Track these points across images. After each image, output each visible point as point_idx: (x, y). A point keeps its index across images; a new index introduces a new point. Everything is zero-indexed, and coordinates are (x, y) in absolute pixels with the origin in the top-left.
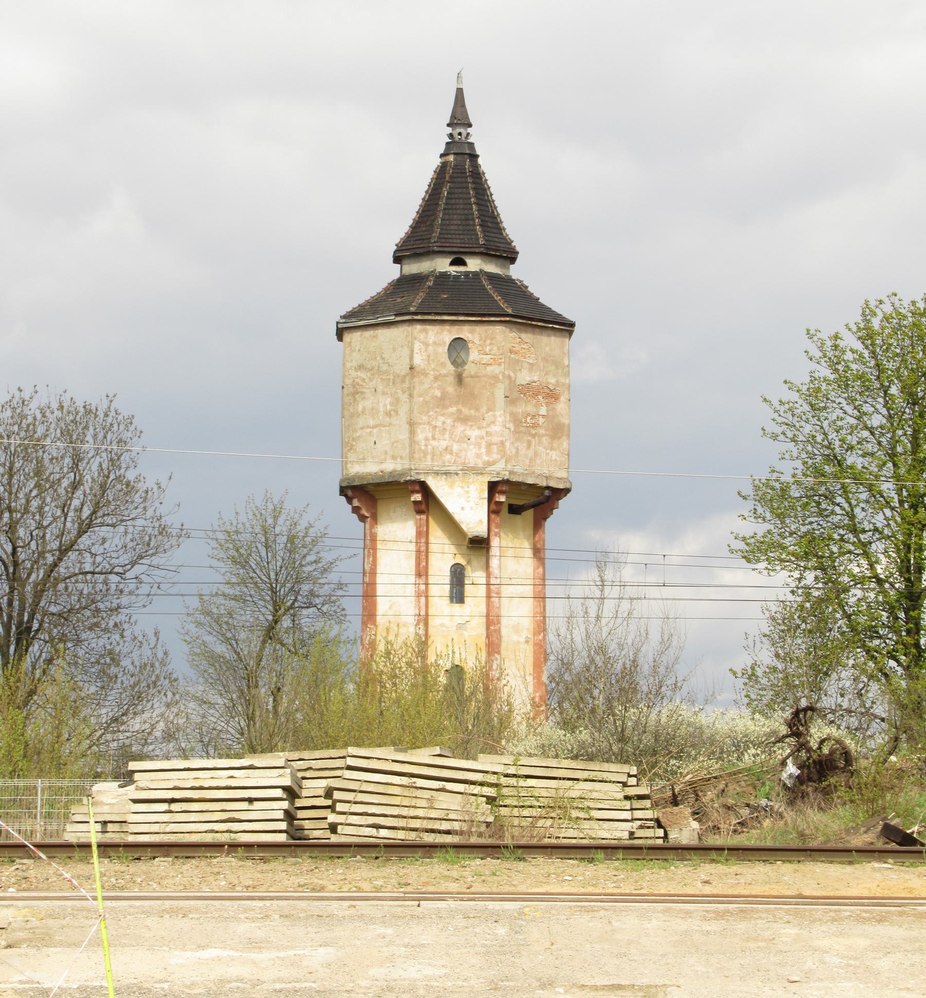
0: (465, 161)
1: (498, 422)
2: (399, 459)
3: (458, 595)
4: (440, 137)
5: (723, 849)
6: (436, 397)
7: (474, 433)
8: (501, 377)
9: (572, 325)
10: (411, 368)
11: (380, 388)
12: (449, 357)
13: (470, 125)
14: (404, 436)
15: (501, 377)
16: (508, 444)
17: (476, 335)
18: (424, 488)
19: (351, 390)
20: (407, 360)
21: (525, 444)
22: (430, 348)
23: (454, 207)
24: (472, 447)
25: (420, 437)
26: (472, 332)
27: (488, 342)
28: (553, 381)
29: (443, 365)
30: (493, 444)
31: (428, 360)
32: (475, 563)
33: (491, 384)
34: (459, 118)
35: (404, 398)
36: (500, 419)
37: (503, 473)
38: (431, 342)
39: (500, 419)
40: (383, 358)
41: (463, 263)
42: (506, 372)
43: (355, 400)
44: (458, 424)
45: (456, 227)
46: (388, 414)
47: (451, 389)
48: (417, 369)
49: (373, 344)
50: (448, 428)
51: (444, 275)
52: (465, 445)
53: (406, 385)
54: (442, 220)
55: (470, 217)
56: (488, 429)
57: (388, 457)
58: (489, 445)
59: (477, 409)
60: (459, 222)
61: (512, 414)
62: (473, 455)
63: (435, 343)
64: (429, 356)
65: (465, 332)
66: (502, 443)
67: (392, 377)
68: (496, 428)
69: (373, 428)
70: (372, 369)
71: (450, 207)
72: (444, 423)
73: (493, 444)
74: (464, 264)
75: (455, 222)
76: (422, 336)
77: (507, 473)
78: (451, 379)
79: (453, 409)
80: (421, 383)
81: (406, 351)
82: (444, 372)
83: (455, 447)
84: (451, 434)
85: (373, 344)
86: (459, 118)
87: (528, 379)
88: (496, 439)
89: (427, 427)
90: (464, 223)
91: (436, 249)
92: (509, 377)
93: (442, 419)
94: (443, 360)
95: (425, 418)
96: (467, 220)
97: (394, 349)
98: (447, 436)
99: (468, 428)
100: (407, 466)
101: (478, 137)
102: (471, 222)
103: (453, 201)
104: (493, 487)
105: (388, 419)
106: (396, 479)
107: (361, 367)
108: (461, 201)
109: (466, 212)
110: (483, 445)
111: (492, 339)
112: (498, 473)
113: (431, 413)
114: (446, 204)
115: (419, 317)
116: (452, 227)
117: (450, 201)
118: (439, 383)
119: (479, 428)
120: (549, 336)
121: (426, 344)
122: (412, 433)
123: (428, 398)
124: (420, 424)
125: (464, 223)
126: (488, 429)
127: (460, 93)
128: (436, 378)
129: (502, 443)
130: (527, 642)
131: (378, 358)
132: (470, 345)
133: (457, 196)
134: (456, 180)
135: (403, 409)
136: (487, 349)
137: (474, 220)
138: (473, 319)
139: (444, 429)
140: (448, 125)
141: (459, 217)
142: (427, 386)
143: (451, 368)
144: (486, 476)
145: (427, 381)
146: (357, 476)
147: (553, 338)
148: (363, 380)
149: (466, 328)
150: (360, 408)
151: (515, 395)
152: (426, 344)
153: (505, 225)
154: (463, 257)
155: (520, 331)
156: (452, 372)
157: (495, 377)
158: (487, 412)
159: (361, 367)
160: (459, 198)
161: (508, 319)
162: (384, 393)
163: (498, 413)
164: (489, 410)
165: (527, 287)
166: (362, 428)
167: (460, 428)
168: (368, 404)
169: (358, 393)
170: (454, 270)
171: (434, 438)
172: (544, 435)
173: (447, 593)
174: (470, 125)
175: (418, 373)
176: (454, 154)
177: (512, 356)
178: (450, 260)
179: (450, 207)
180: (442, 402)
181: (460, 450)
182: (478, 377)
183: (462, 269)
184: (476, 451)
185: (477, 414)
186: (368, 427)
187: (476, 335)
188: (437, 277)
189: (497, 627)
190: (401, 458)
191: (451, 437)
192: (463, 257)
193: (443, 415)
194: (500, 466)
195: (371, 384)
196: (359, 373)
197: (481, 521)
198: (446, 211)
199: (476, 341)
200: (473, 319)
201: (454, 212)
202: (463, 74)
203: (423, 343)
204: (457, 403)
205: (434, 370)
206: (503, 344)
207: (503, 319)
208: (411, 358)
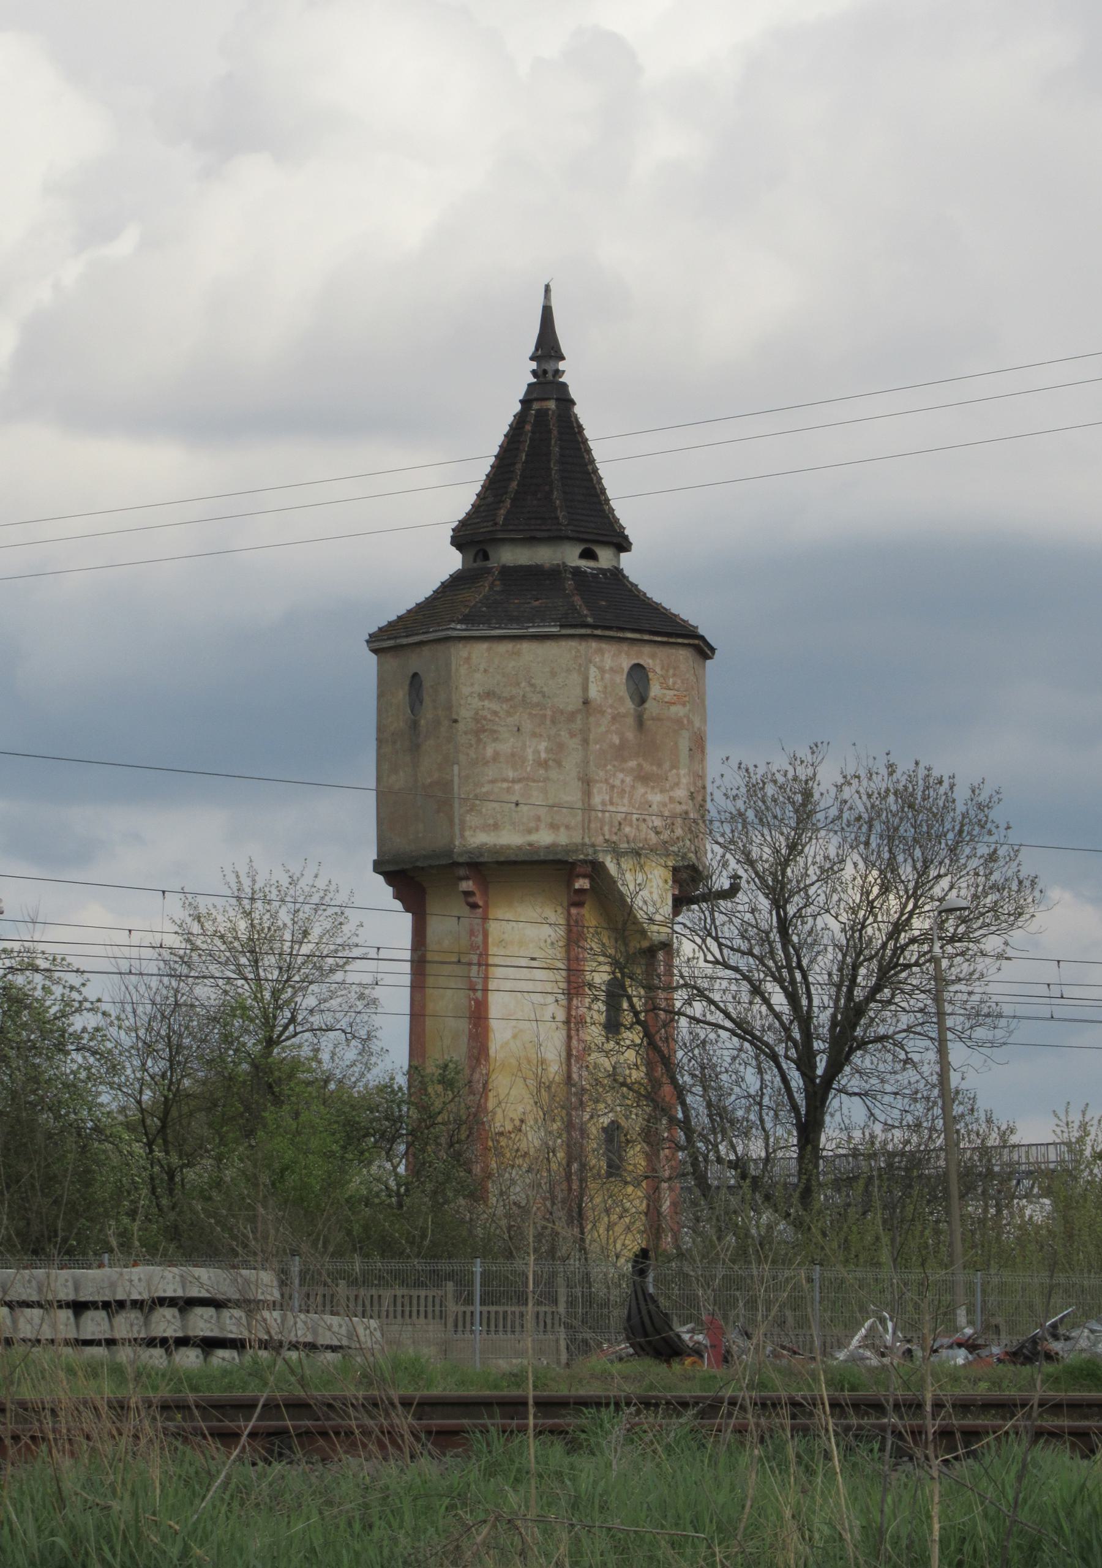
2: (562, 829)
5: (685, 1405)
8: (685, 722)
9: (713, 650)
10: (586, 702)
11: (528, 726)
13: (563, 358)
14: (572, 795)
15: (685, 722)
18: (596, 870)
20: (578, 691)
22: (607, 676)
25: (597, 800)
26: (653, 656)
27: (671, 672)
29: (621, 700)
31: (605, 693)
34: (547, 348)
35: (573, 743)
36: (684, 781)
40: (532, 685)
43: (479, 741)
44: (639, 785)
46: (544, 764)
47: (630, 735)
49: (512, 664)
50: (628, 789)
51: (577, 572)
53: (578, 724)
56: (671, 794)
57: (543, 825)
59: (660, 765)
63: (611, 669)
64: (605, 687)
67: (549, 713)
69: (513, 781)
70: (512, 698)
72: (623, 781)
78: (630, 721)
79: (632, 764)
81: (576, 678)
82: (622, 710)
84: (631, 798)
86: (547, 348)
89: (604, 787)
91: (570, 533)
93: (621, 776)
94: (621, 694)
95: (602, 773)
97: (553, 674)
98: (626, 801)
100: (578, 840)
101: (574, 373)
105: (542, 771)
106: (559, 857)
107: (489, 695)
111: (675, 669)
113: (609, 767)
115: (598, 632)
119: (662, 791)
122: (588, 794)
124: (597, 781)
126: (671, 794)
128: (614, 718)
131: (523, 684)
132: (651, 675)
135: (572, 762)
138: (659, 639)
139: (623, 791)
140: (532, 359)
142: (603, 729)
145: (605, 720)
146: (480, 850)
148: (495, 713)
149: (647, 649)
150: (489, 752)
152: (602, 670)
157: (679, 721)
158: (670, 770)
159: (489, 695)
162: (534, 735)
166: (493, 782)
168: (505, 747)
169: (485, 731)
170: (584, 564)
171: (612, 803)
174: (563, 358)
176: (557, 400)
180: (620, 752)
183: (592, 564)
186: (504, 780)
190: (567, 827)
193: (622, 770)
195: (510, 720)
196: (486, 703)
199: (658, 670)
200: (659, 639)
203: (598, 668)
205: (611, 706)
208: (585, 689)
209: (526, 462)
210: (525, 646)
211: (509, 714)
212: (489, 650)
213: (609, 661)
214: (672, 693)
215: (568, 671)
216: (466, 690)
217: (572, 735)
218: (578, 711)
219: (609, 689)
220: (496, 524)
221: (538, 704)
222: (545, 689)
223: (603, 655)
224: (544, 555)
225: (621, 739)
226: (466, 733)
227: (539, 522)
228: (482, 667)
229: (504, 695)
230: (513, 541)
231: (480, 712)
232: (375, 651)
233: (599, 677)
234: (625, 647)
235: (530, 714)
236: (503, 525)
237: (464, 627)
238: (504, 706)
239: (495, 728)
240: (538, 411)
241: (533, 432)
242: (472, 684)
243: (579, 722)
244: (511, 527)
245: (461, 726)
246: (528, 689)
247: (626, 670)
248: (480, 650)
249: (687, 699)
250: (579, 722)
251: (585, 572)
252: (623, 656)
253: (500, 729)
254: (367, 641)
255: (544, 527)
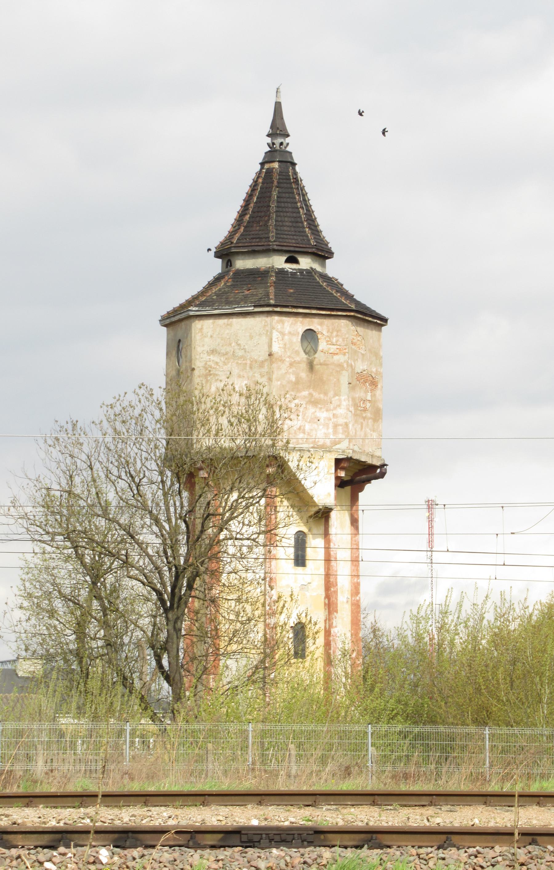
0: (288, 168)
1: (343, 406)
3: (300, 560)
4: (261, 146)
6: (292, 381)
7: (323, 415)
8: (345, 366)
9: (385, 320)
10: (270, 355)
11: (236, 371)
12: (302, 346)
13: (288, 136)
15: (345, 366)
16: (350, 426)
17: (325, 327)
19: (203, 372)
20: (266, 347)
21: (360, 426)
22: (286, 337)
23: (284, 210)
24: (321, 427)
26: (321, 324)
27: (335, 334)
28: (374, 370)
29: (297, 353)
30: (339, 425)
31: (285, 348)
32: (315, 531)
33: (337, 371)
34: (278, 129)
36: (344, 403)
37: (348, 451)
38: (286, 332)
39: (344, 403)
40: (239, 345)
41: (296, 261)
42: (350, 362)
43: (207, 381)
45: (288, 229)
47: (304, 375)
48: (275, 356)
49: (227, 331)
51: (281, 272)
52: (315, 426)
53: (265, 369)
54: (276, 221)
55: (299, 220)
56: (334, 412)
58: (336, 426)
59: (326, 394)
60: (290, 224)
61: (354, 399)
62: (322, 433)
64: (285, 345)
65: (315, 324)
66: (346, 425)
67: (248, 362)
68: (341, 411)
70: (227, 353)
71: (280, 209)
73: (339, 425)
74: (296, 261)
75: (287, 224)
76: (279, 326)
77: (351, 451)
79: (305, 393)
80: (279, 368)
81: (264, 339)
82: (298, 359)
83: (307, 427)
84: (304, 415)
85: (227, 331)
86: (278, 129)
87: (361, 368)
88: (341, 421)
90: (294, 224)
92: (351, 366)
94: (297, 348)
96: (297, 222)
97: (251, 337)
99: (318, 410)
101: (295, 146)
102: (300, 225)
103: (283, 205)
104: (338, 462)
107: (213, 352)
108: (289, 205)
109: (295, 215)
110: (331, 425)
111: (337, 332)
112: (343, 452)
114: (277, 207)
115: (278, 309)
116: (285, 228)
117: (280, 205)
118: (294, 369)
119: (327, 410)
120: (372, 330)
121: (283, 334)
123: (284, 382)
125: (294, 224)
126: (334, 412)
127: (278, 107)
128: (291, 365)
129: (346, 425)
130: (347, 602)
131: (233, 344)
133: (285, 200)
134: (282, 185)
136: (334, 340)
137: (302, 223)
138: (324, 312)
140: (268, 135)
141: (290, 220)
142: (283, 371)
143: (303, 356)
144: (333, 453)
145: (284, 367)
147: (374, 332)
148: (217, 363)
149: (316, 321)
151: (355, 382)
152: (283, 334)
153: (321, 228)
154: (296, 256)
155: (357, 325)
156: (305, 360)
157: (340, 365)
158: (334, 396)
159: (213, 352)
160: (287, 202)
161: (352, 314)
162: (239, 376)
163: (343, 398)
164: (336, 395)
165: (342, 285)
167: (311, 410)
169: (210, 375)
170: (289, 267)
172: (370, 418)
173: (292, 557)
174: (288, 136)
175: (276, 359)
176: (279, 161)
177: (353, 347)
178: (285, 258)
179: (280, 209)
181: (311, 430)
182: (327, 365)
183: (294, 266)
184: (324, 430)
185: (326, 398)
187: (325, 327)
188: (277, 273)
189: (335, 589)
191: (303, 418)
192: (296, 256)
194: (344, 445)
195: (225, 367)
197: (329, 494)
198: (278, 214)
199: (325, 332)
200: (324, 312)
201: (285, 214)
202: (281, 89)
204: (309, 387)
205: (289, 357)
206: (347, 336)
207: (348, 314)
208: (270, 346)
209: (256, 203)
210: (235, 321)
211: (225, 364)
212: (213, 323)
213: (288, 328)
214: (335, 347)
215: (260, 335)
216: (199, 349)
217: (262, 376)
218: (266, 360)
219: (288, 346)
220: (232, 243)
221: (242, 357)
222: (246, 347)
223: (283, 324)
224: (261, 262)
225: (297, 378)
226: (199, 377)
227: (258, 240)
228: (209, 334)
229: (222, 351)
230: (243, 253)
231: (208, 363)
232: (165, 326)
233: (280, 338)
234: (300, 319)
235: (237, 363)
236: (236, 243)
237: (197, 309)
238: (222, 359)
239: (217, 373)
240: (268, 169)
241: (263, 183)
242: (203, 345)
243: (266, 367)
244: (240, 245)
245: (196, 373)
246: (236, 347)
247: (301, 333)
248: (208, 323)
249: (347, 351)
250: (266, 367)
251: (287, 271)
252: (299, 324)
253: (220, 373)
254: (160, 321)
255: (259, 244)
